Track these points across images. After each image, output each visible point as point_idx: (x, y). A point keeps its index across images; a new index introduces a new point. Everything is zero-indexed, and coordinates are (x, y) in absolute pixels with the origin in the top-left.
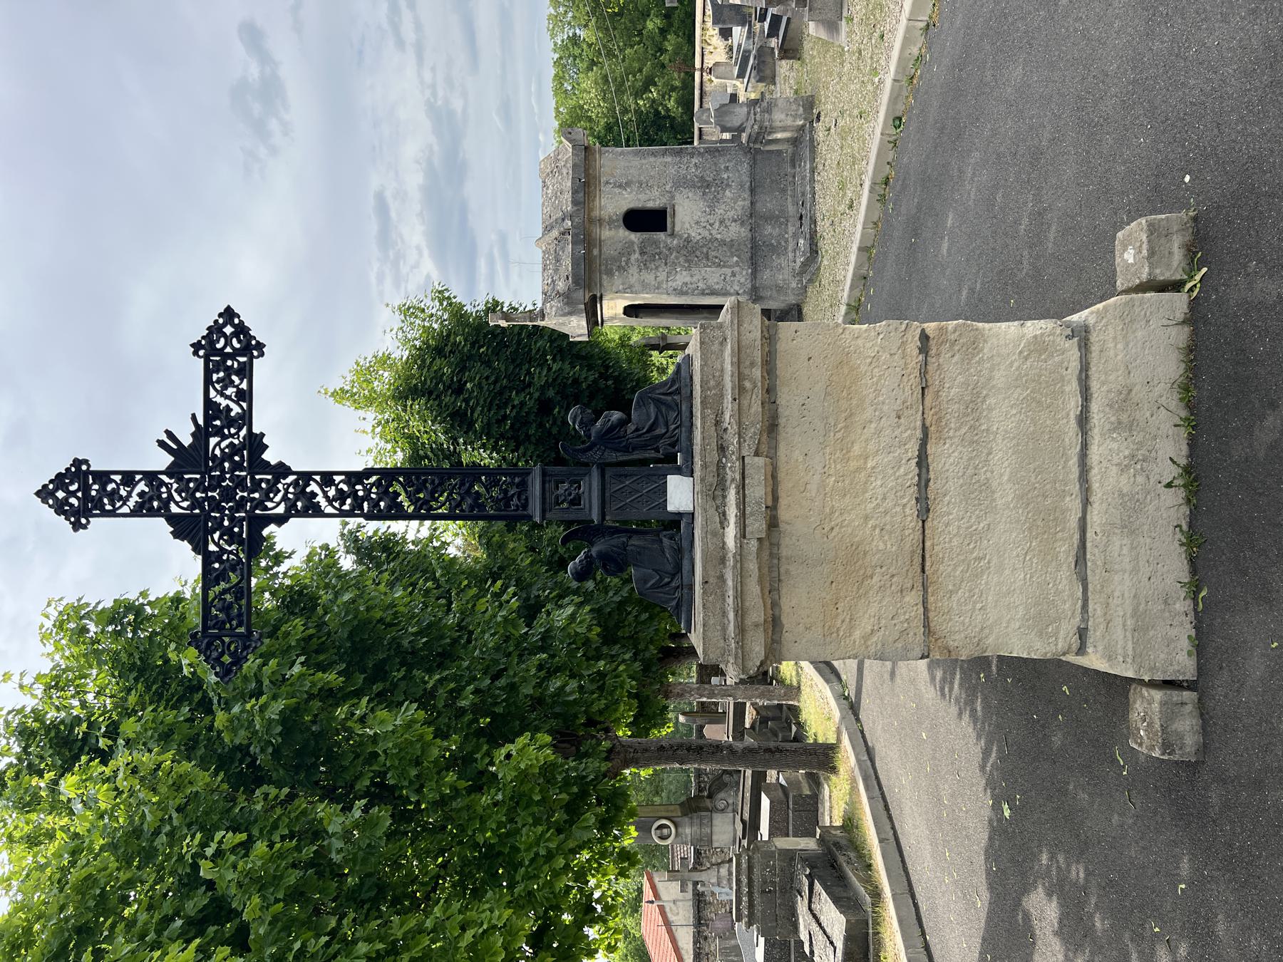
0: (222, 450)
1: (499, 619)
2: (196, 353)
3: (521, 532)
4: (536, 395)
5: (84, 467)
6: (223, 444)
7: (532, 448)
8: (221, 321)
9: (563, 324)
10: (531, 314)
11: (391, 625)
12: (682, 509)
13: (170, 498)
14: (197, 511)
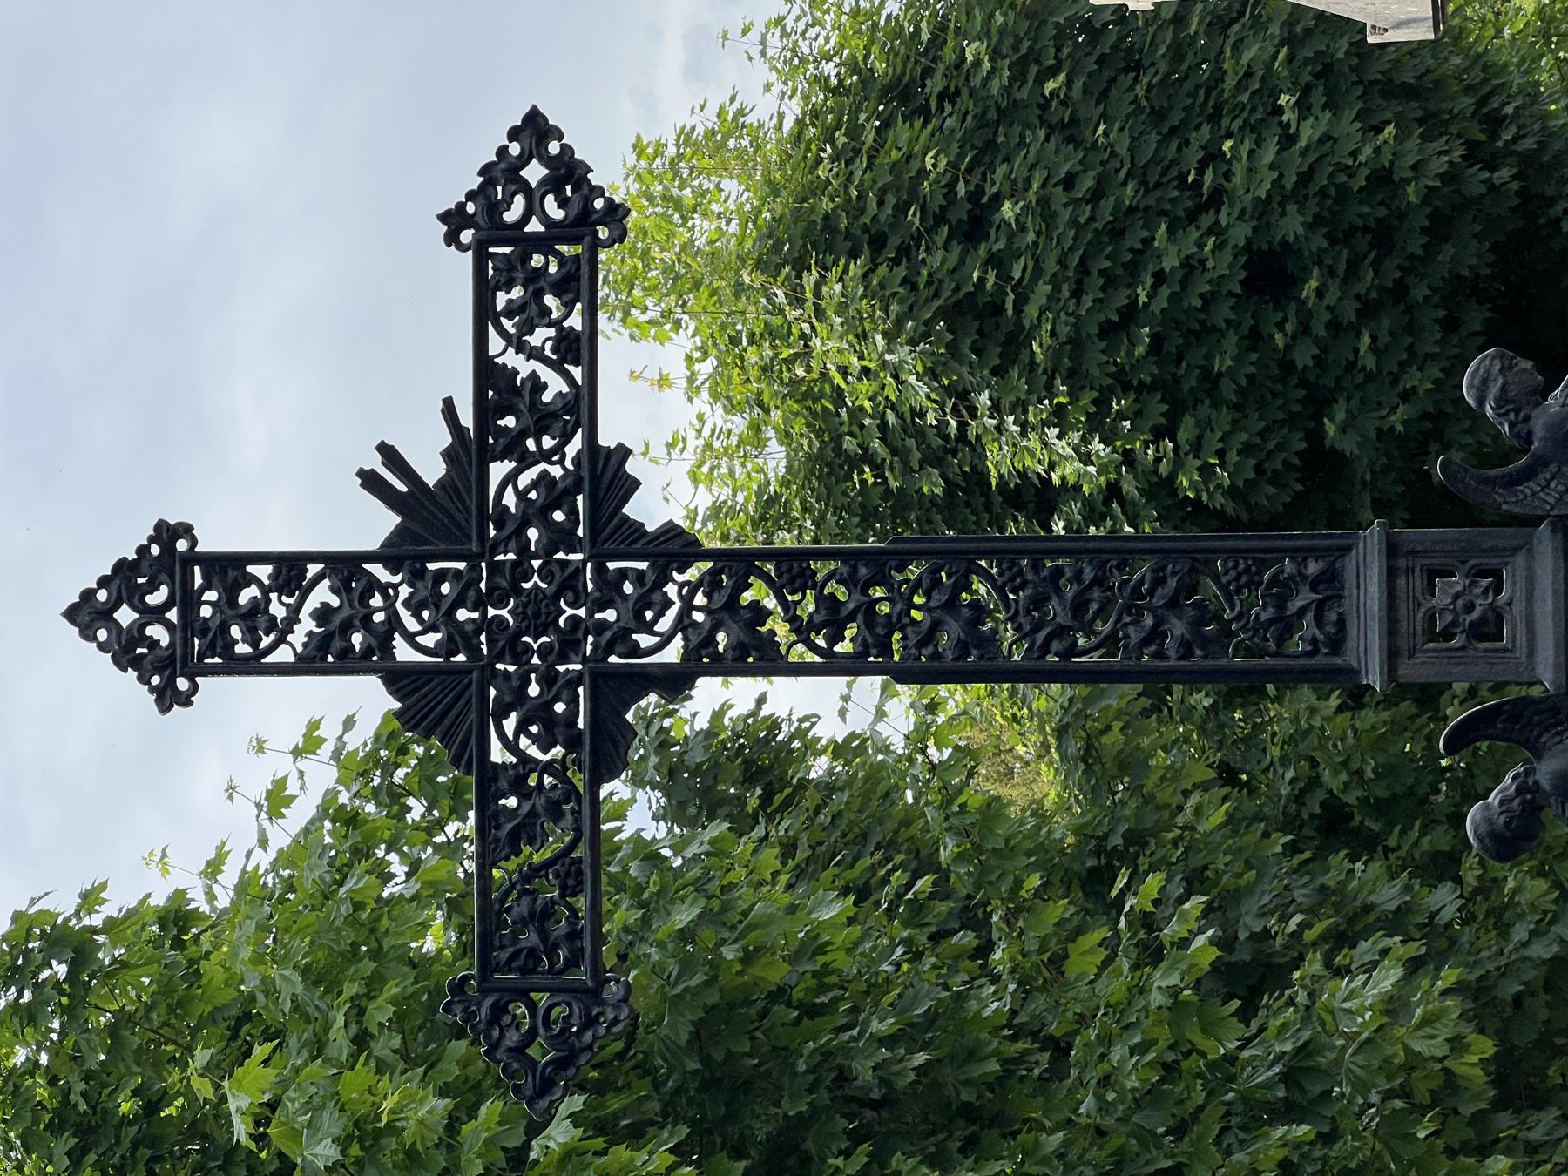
0: (521, 495)
1: (1156, 999)
2: (452, 239)
3: (1187, 714)
4: (1240, 234)
5: (182, 545)
6: (525, 480)
7: (1224, 418)
8: (515, 149)
11: (811, 1011)
13: (394, 623)
14: (461, 658)
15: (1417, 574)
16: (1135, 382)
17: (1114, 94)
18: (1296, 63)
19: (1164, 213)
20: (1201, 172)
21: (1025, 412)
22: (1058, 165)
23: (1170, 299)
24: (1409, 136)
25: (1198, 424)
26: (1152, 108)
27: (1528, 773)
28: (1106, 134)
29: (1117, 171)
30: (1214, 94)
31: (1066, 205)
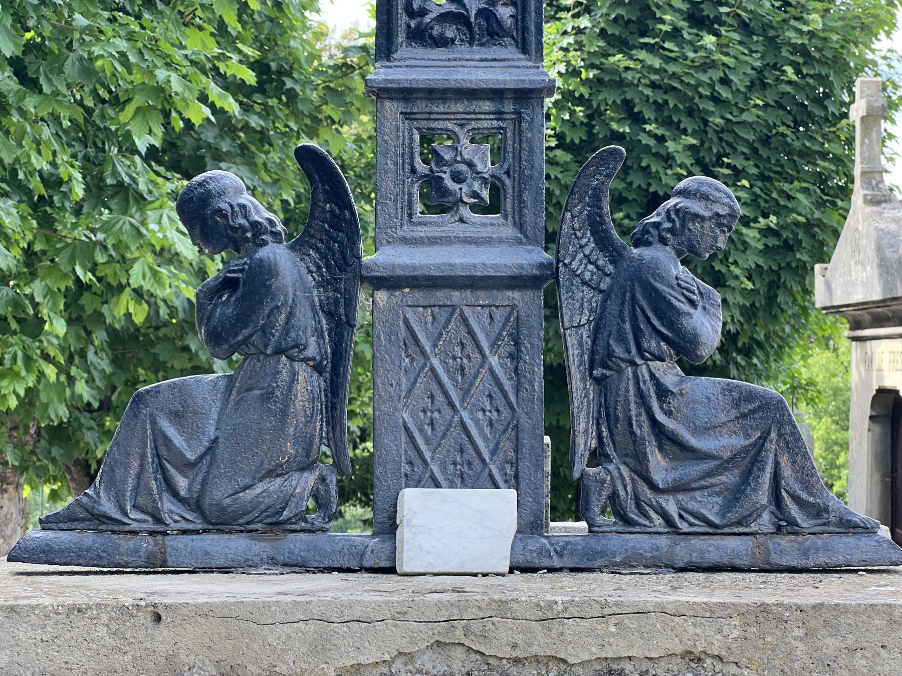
1: (161, 74)
9: (857, 249)
10: (874, 174)
12: (404, 533)
15: (495, 123)
16: (594, 123)
17: (781, 112)
18: (794, 228)
19: (702, 143)
20: (729, 166)
21: (576, 50)
22: (738, 74)
23: (647, 145)
24: (744, 298)
25: (566, 163)
26: (769, 137)
27: (276, 235)
28: (756, 106)
29: (731, 113)
30: (777, 177)
31: (711, 79)
